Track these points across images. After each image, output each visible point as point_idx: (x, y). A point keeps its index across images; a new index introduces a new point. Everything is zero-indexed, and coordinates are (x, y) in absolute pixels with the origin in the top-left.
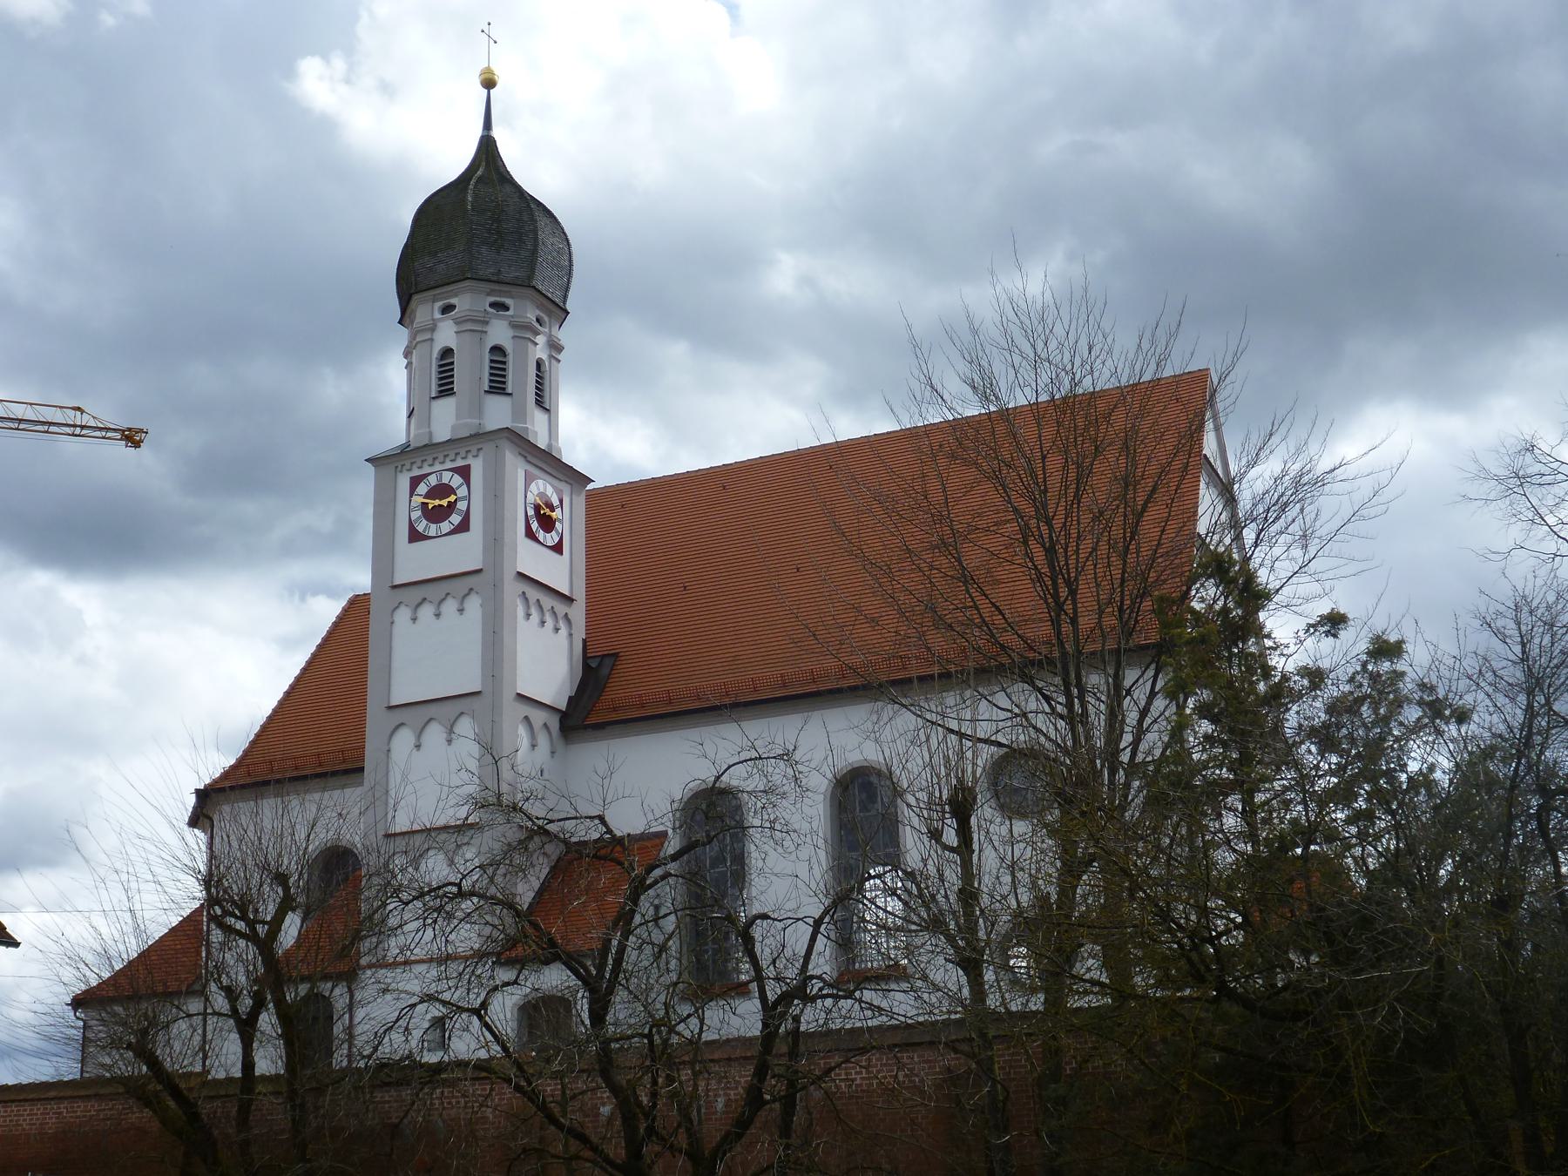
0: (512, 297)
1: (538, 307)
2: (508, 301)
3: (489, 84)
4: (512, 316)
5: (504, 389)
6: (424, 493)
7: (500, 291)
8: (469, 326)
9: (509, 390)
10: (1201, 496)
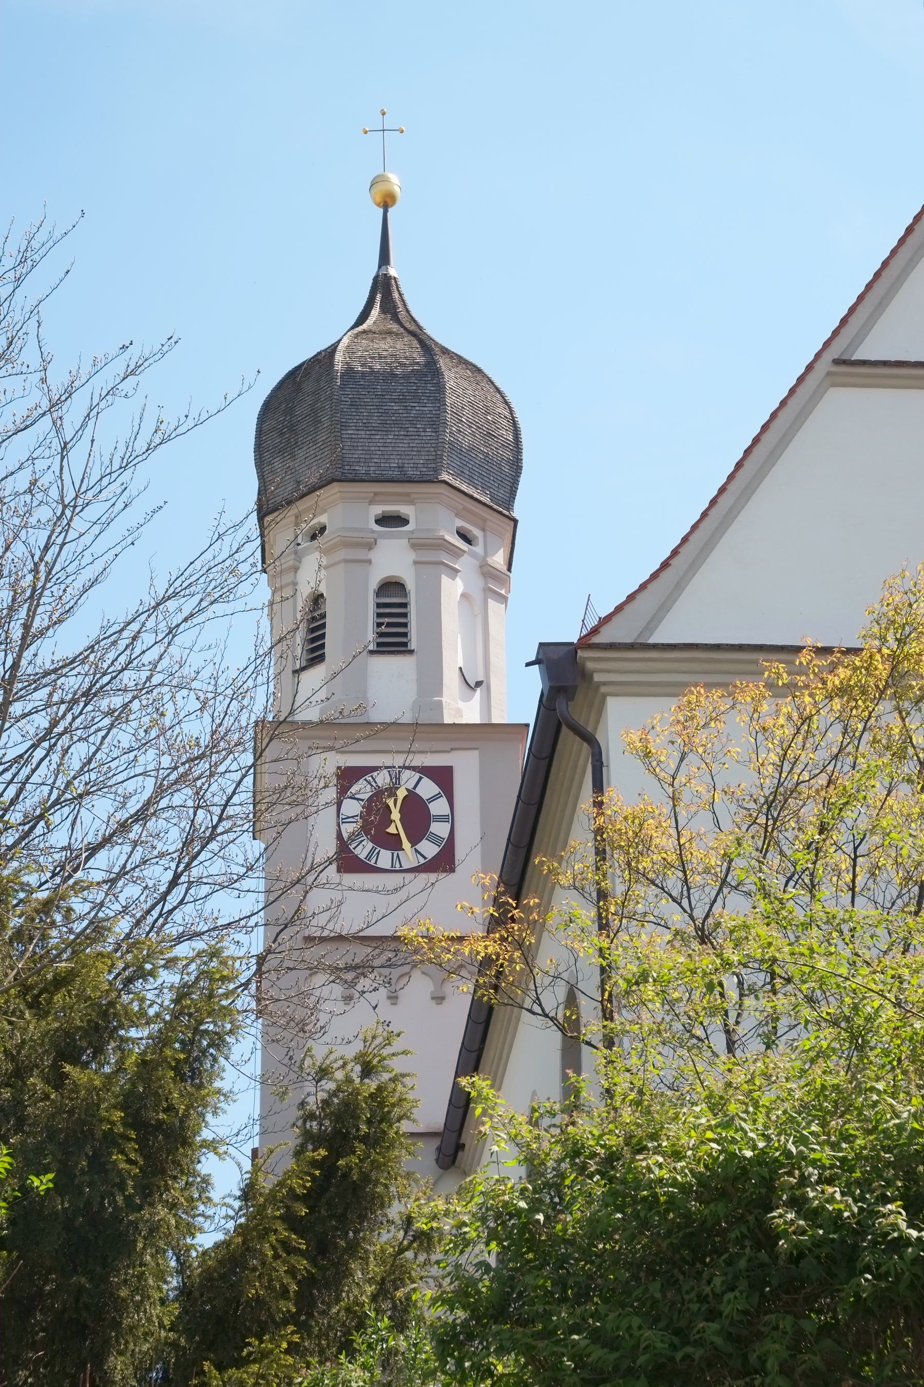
0: (411, 502)
1: (457, 515)
2: (404, 510)
3: (387, 202)
4: (412, 532)
5: (405, 644)
6: (418, 791)
7: (389, 494)
8: (342, 554)
9: (413, 645)
10: (303, 627)
